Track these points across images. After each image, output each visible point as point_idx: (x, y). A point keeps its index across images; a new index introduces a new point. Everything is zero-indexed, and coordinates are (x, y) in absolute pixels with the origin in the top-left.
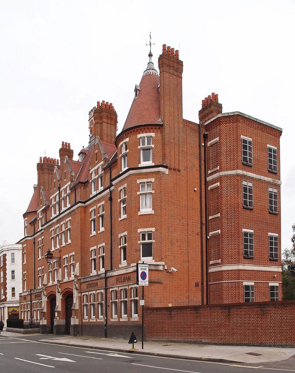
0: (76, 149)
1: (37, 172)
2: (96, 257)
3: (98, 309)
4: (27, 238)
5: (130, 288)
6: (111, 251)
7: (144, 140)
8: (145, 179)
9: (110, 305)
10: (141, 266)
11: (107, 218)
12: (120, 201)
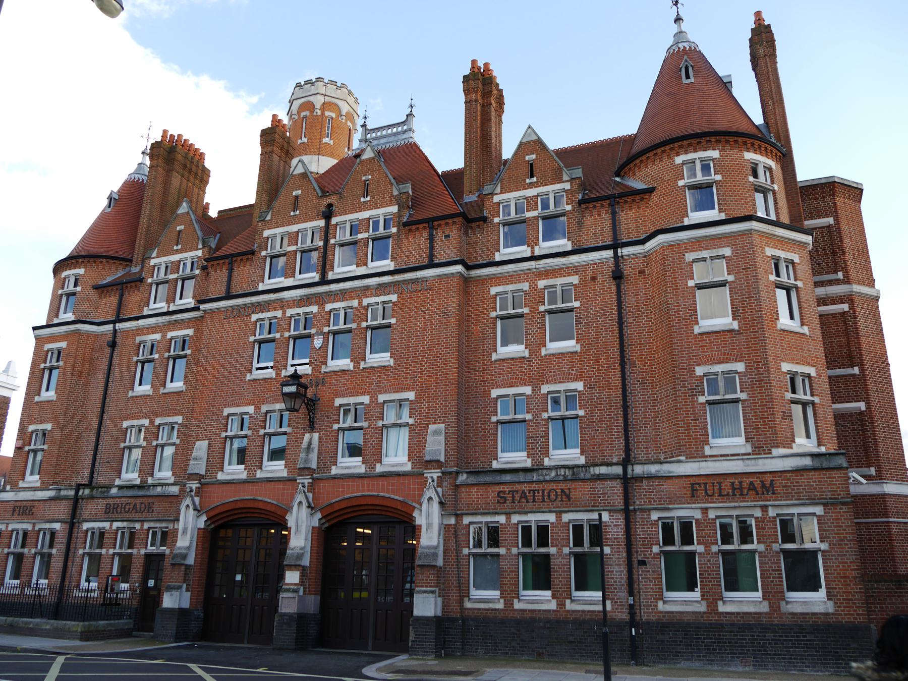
3: (112, 565)
6: (625, 407)
7: (306, 235)
8: (704, 252)
9: (78, 560)
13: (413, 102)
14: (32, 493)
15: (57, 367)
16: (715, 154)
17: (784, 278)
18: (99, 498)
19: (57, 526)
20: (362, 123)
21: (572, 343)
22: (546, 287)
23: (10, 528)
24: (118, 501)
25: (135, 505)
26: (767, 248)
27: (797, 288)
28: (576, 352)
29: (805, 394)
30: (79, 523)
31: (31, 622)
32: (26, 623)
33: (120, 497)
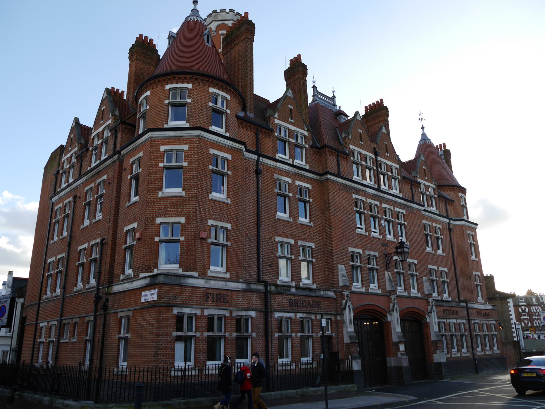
4: (149, 133)
13: (334, 89)
14: (223, 283)
16: (190, 86)
17: (220, 168)
18: (283, 294)
19: (253, 314)
20: (313, 85)
21: (180, 190)
22: (166, 151)
23: (206, 312)
24: (297, 298)
25: (309, 302)
26: (210, 149)
28: (181, 197)
30: (271, 312)
31: (318, 391)
32: (315, 391)
33: (298, 295)
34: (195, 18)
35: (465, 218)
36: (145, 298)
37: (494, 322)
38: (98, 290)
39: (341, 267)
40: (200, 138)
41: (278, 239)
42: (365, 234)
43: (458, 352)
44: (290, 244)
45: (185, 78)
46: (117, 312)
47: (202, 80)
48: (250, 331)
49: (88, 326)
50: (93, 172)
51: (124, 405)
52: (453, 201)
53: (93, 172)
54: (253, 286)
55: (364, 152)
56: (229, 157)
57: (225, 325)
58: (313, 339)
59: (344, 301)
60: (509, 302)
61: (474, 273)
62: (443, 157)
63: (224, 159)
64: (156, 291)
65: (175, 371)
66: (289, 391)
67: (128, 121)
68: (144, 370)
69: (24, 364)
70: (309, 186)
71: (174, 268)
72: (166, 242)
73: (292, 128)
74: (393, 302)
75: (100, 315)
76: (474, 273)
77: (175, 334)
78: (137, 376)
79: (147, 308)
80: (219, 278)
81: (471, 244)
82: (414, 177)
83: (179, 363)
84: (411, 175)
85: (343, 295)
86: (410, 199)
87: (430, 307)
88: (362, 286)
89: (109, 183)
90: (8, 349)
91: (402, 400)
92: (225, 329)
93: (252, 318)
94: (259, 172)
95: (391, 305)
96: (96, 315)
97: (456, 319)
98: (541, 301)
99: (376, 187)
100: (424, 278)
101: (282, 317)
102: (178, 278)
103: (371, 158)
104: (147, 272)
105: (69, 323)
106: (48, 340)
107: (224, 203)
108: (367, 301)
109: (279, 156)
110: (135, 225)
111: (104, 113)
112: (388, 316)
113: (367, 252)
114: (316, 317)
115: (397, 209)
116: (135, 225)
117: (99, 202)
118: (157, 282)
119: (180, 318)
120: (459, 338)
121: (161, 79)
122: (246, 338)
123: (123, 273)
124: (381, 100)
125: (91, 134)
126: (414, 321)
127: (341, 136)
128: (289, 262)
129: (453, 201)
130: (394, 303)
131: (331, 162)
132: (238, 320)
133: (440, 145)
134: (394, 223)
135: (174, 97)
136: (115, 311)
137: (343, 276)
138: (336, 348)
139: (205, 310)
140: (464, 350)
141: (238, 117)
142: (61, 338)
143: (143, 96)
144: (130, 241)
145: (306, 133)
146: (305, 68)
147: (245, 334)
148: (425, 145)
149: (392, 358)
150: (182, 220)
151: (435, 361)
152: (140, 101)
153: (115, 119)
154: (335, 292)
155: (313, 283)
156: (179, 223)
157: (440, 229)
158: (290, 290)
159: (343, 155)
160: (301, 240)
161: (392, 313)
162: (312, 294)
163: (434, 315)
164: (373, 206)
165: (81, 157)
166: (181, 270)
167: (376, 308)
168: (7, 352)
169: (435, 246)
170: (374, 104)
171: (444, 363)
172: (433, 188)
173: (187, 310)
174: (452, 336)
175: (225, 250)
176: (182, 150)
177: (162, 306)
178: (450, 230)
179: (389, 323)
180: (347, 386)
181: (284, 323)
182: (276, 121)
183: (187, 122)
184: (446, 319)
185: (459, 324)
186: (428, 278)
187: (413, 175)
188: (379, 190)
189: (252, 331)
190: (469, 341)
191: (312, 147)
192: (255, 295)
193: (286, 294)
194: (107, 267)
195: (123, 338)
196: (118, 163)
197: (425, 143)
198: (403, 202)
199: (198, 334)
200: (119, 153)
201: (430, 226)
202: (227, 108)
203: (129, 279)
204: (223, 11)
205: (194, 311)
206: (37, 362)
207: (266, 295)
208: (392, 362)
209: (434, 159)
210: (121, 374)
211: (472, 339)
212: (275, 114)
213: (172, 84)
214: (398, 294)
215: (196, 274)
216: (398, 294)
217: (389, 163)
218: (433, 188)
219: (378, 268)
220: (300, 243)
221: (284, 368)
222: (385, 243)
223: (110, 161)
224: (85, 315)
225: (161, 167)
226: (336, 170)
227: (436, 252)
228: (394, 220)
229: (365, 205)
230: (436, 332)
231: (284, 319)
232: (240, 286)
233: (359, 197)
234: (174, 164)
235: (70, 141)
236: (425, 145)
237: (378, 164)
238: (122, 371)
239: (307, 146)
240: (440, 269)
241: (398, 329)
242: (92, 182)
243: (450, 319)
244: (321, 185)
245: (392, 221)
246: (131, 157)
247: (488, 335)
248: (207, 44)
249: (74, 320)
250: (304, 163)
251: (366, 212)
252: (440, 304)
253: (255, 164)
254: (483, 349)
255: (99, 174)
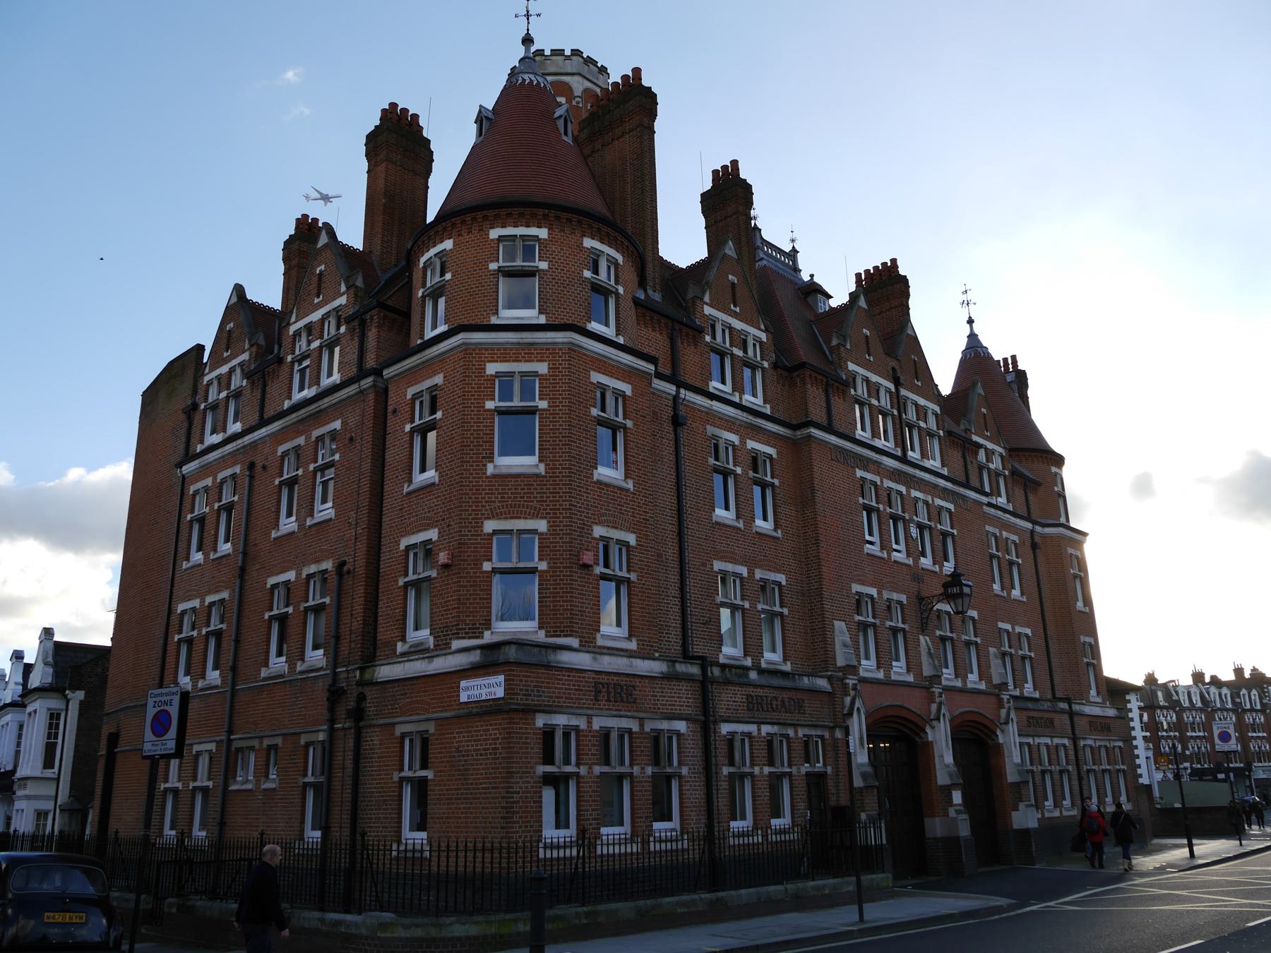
0: (451, 149)
1: (365, 165)
2: (195, 633)
4: (461, 336)
5: (265, 745)
10: (156, 696)
11: (238, 515)
12: (412, 431)
13: (795, 235)
15: (431, 426)
16: (543, 233)
17: (609, 413)
19: (681, 726)
21: (533, 460)
22: (498, 375)
23: (597, 723)
24: (760, 692)
25: (783, 701)
27: (625, 428)
28: (537, 475)
29: (621, 569)
30: (715, 723)
31: (825, 886)
32: (818, 888)
33: (762, 687)
34: (532, 77)
35: (1063, 520)
36: (470, 693)
37: (1121, 744)
38: (335, 674)
39: (839, 625)
40: (573, 349)
41: (718, 565)
42: (879, 554)
43: (1055, 806)
44: (739, 576)
45: (534, 216)
46: (393, 724)
47: (569, 220)
48: (675, 763)
49: (307, 754)
50: (303, 412)
51: (475, 918)
52: (1038, 484)
53: (303, 411)
54: (681, 668)
55: (874, 378)
56: (627, 388)
57: (631, 751)
58: (791, 780)
59: (848, 700)
60: (1129, 701)
61: (1082, 639)
62: (1015, 387)
63: (618, 394)
64: (501, 678)
65: (545, 848)
66: (772, 888)
67: (389, 303)
68: (448, 846)
69: (117, 839)
70: (771, 451)
71: (525, 628)
72: (501, 573)
73: (738, 325)
74: (937, 700)
75: (344, 729)
76: (1082, 639)
77: (542, 769)
78: (452, 860)
79: (478, 714)
80: (617, 649)
81: (1075, 576)
82: (966, 430)
83: (550, 833)
84: (958, 424)
85: (845, 686)
86: (962, 479)
87: (1003, 712)
88: (878, 668)
89: (351, 439)
90: (49, 805)
91: (992, 904)
92: (631, 760)
93: (679, 734)
94: (681, 420)
95: (934, 707)
96: (332, 732)
97: (1052, 737)
98: (1175, 698)
99: (899, 453)
100: (992, 650)
101: (733, 734)
102: (543, 651)
103: (888, 391)
104: (470, 638)
105: (251, 748)
106: (192, 785)
107: (621, 489)
108: (888, 699)
109: (715, 385)
110: (433, 534)
111: (324, 279)
112: (928, 730)
113: (886, 595)
114: (796, 732)
115: (939, 502)
116: (433, 534)
117: (319, 480)
118: (502, 659)
119: (548, 734)
120: (1057, 776)
121: (480, 215)
122: (669, 778)
123: (403, 639)
124: (894, 261)
125: (289, 324)
126: (976, 741)
127: (828, 342)
128: (739, 615)
129: (1038, 484)
130: (940, 703)
131: (815, 397)
132: (656, 737)
133: (1005, 360)
134: (934, 532)
135: (510, 256)
136: (387, 721)
137: (845, 645)
138: (834, 798)
139: (595, 720)
140: (1067, 803)
141: (636, 302)
142: (231, 781)
143: (433, 252)
144: (418, 570)
145: (763, 337)
146: (746, 189)
147: (669, 770)
148: (974, 356)
149: (937, 819)
150: (542, 525)
151: (1015, 827)
152: (423, 260)
153: (356, 296)
154: (829, 679)
155: (785, 660)
156: (535, 531)
157: (1016, 544)
158: (747, 676)
159: (838, 385)
160: (760, 567)
161: (935, 723)
162: (788, 684)
163: (1013, 728)
164: (893, 495)
165: (263, 377)
166: (542, 634)
167: (904, 714)
168: (46, 813)
169: (1007, 580)
170: (876, 268)
171: (1034, 829)
172: (1001, 455)
173: (561, 720)
174: (1061, 772)
175: (624, 590)
176: (535, 374)
177: (516, 710)
178: (1034, 546)
179: (928, 746)
180: (874, 876)
181: (737, 744)
182: (708, 310)
183: (540, 313)
184: (1033, 736)
185: (1057, 746)
186: (998, 649)
187: (962, 427)
188: (903, 459)
189: (680, 763)
190: (1075, 783)
191: (775, 366)
192: (684, 686)
193: (742, 685)
194: (357, 624)
195: (408, 779)
196: (372, 396)
197: (977, 354)
198: (949, 485)
199: (583, 770)
200: (377, 372)
201: (996, 537)
202: (617, 282)
203: (419, 651)
204: (557, 52)
205: (574, 721)
206: (161, 835)
207: (704, 686)
208: (936, 827)
209: (994, 386)
210: (413, 857)
211: (1080, 779)
212: (703, 293)
213: (504, 226)
214: (944, 683)
215: (574, 642)
216: (944, 683)
217: (922, 402)
218: (1001, 455)
219: (906, 627)
220: (759, 574)
221: (561, 854)
222: (919, 575)
223: (352, 389)
224: (298, 730)
225: (489, 410)
226: (824, 415)
227: (1009, 594)
228: (932, 524)
229: (880, 492)
230: (1017, 765)
231: (738, 738)
232: (655, 667)
233: (869, 476)
234: (516, 403)
235: (225, 338)
236: (974, 356)
237: (899, 402)
238: (414, 851)
239: (766, 364)
240: (1018, 629)
241: (949, 759)
242: (299, 434)
243: (1039, 736)
244: (797, 450)
245: (930, 528)
246: (410, 384)
247: (1109, 771)
248: (565, 138)
249: (266, 742)
250: (759, 401)
251: (881, 507)
252: (1021, 704)
253: (671, 403)
254: (1057, 805)
255: (319, 418)
